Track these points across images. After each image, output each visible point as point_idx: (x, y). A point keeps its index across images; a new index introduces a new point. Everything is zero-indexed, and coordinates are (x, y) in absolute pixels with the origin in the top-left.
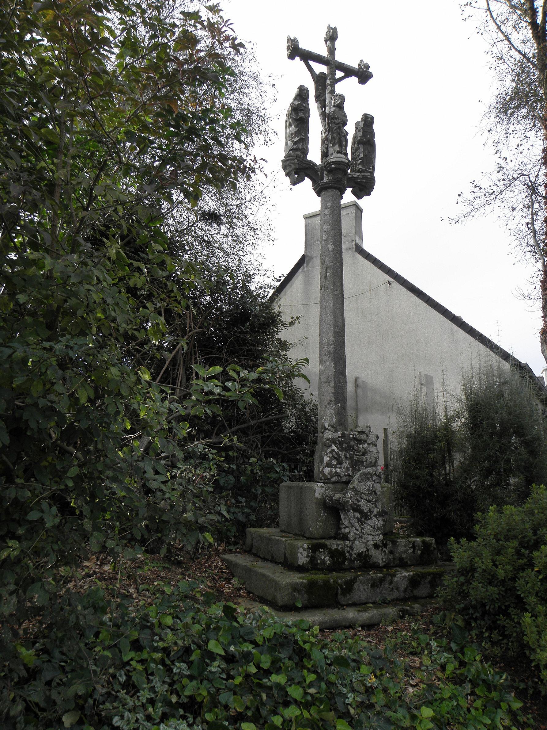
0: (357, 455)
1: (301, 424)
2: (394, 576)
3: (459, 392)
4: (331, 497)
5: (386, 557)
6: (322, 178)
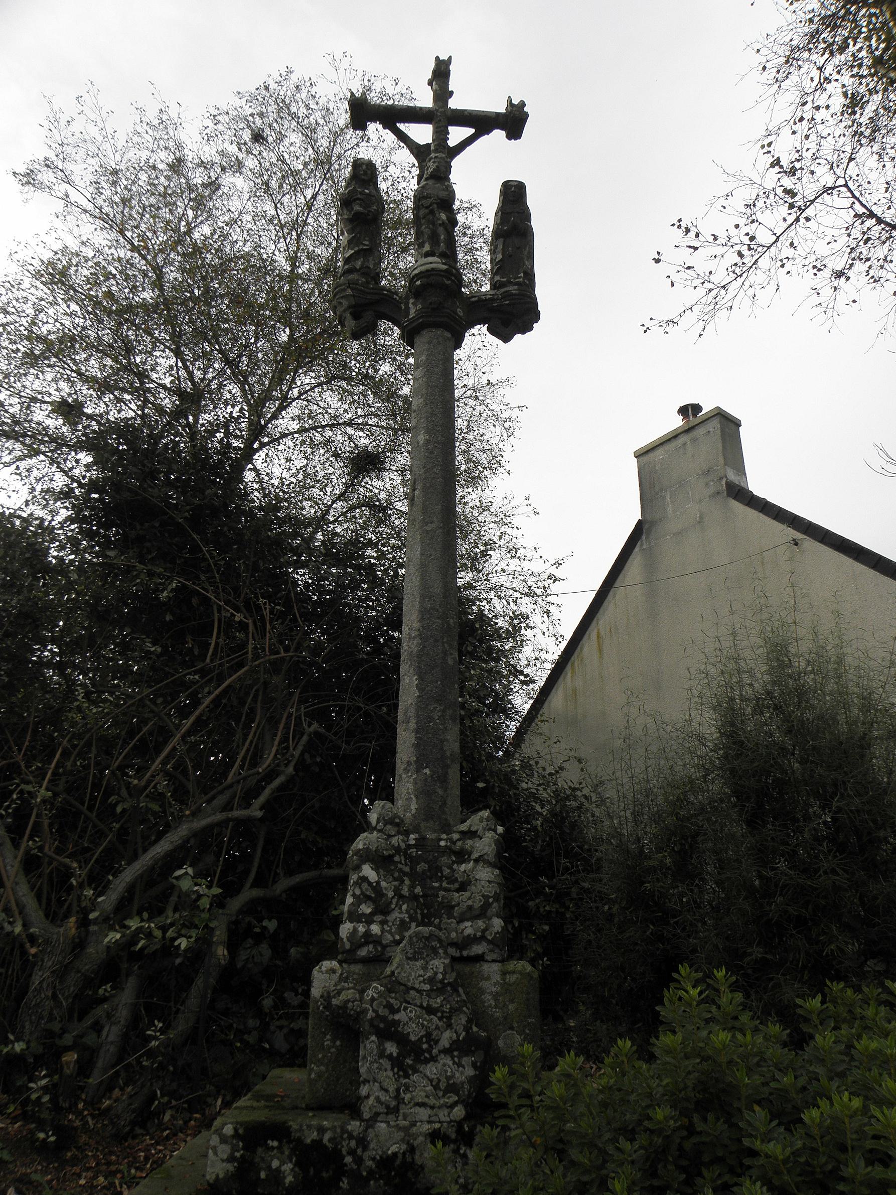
0: (446, 890)
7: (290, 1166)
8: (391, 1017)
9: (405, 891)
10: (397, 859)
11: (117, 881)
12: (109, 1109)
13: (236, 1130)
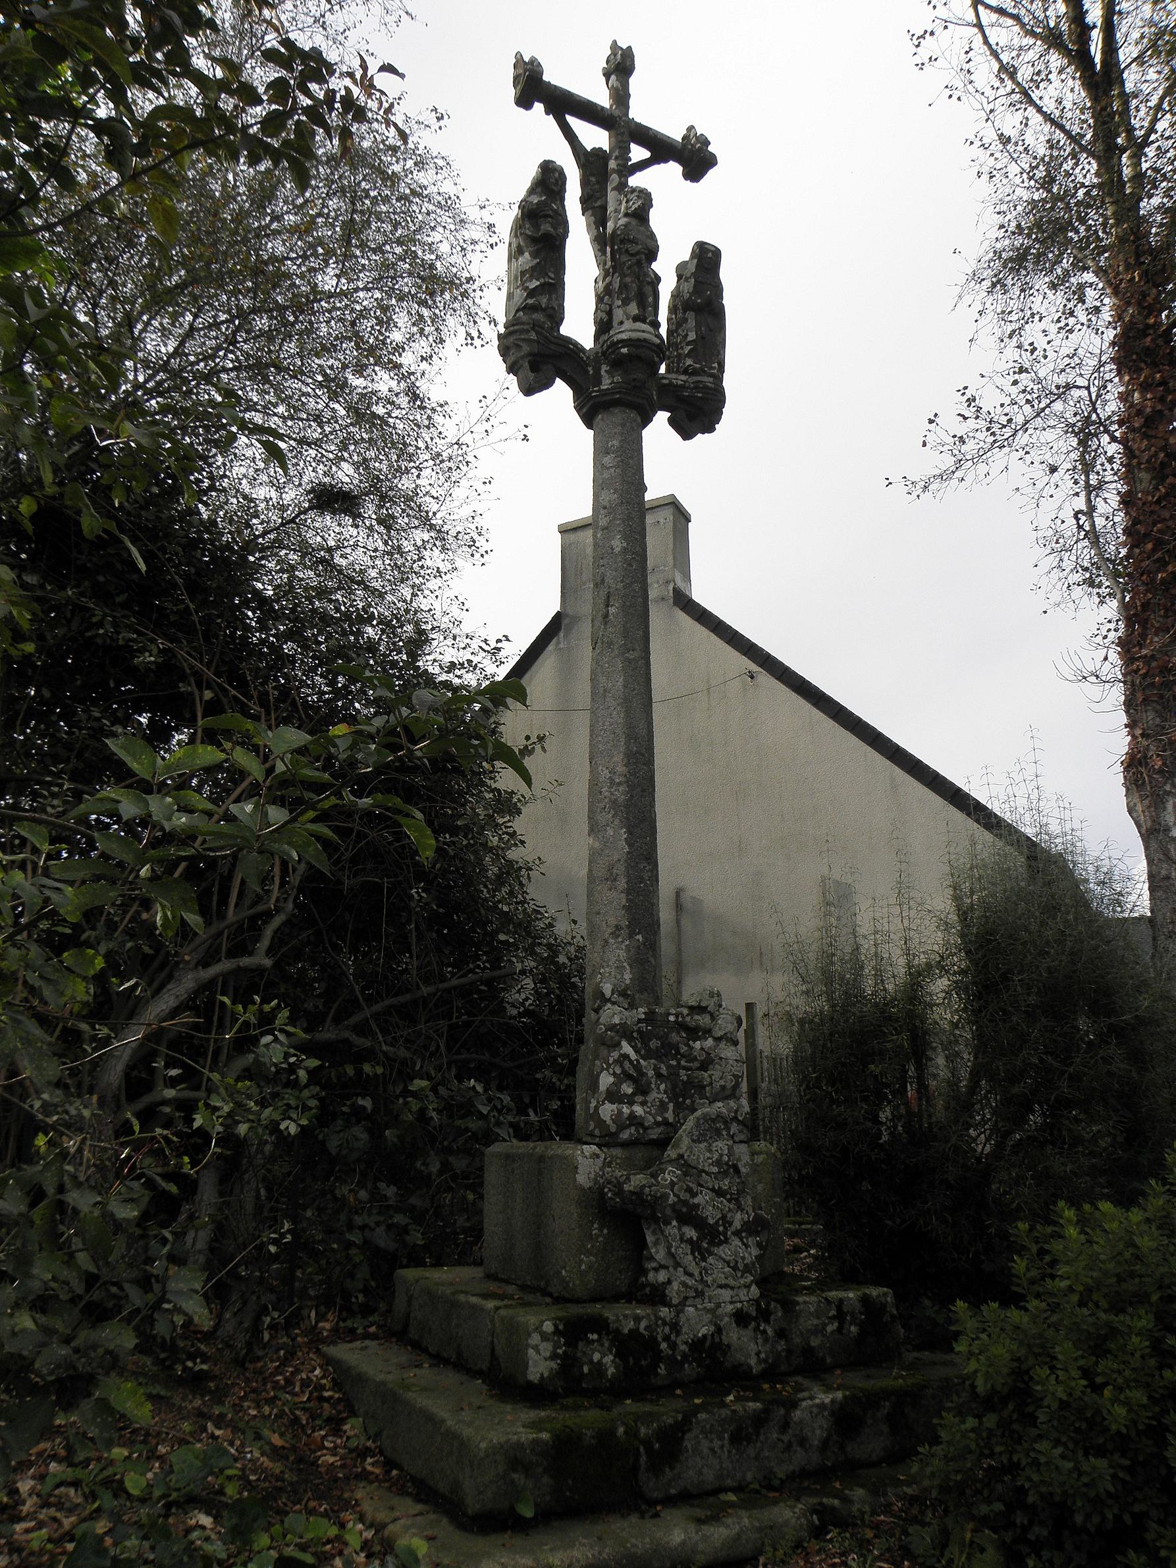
0: (685, 1068)
1: (548, 994)
2: (793, 1404)
3: (942, 903)
4: (619, 1185)
6: (598, 382)
13: (556, 1326)
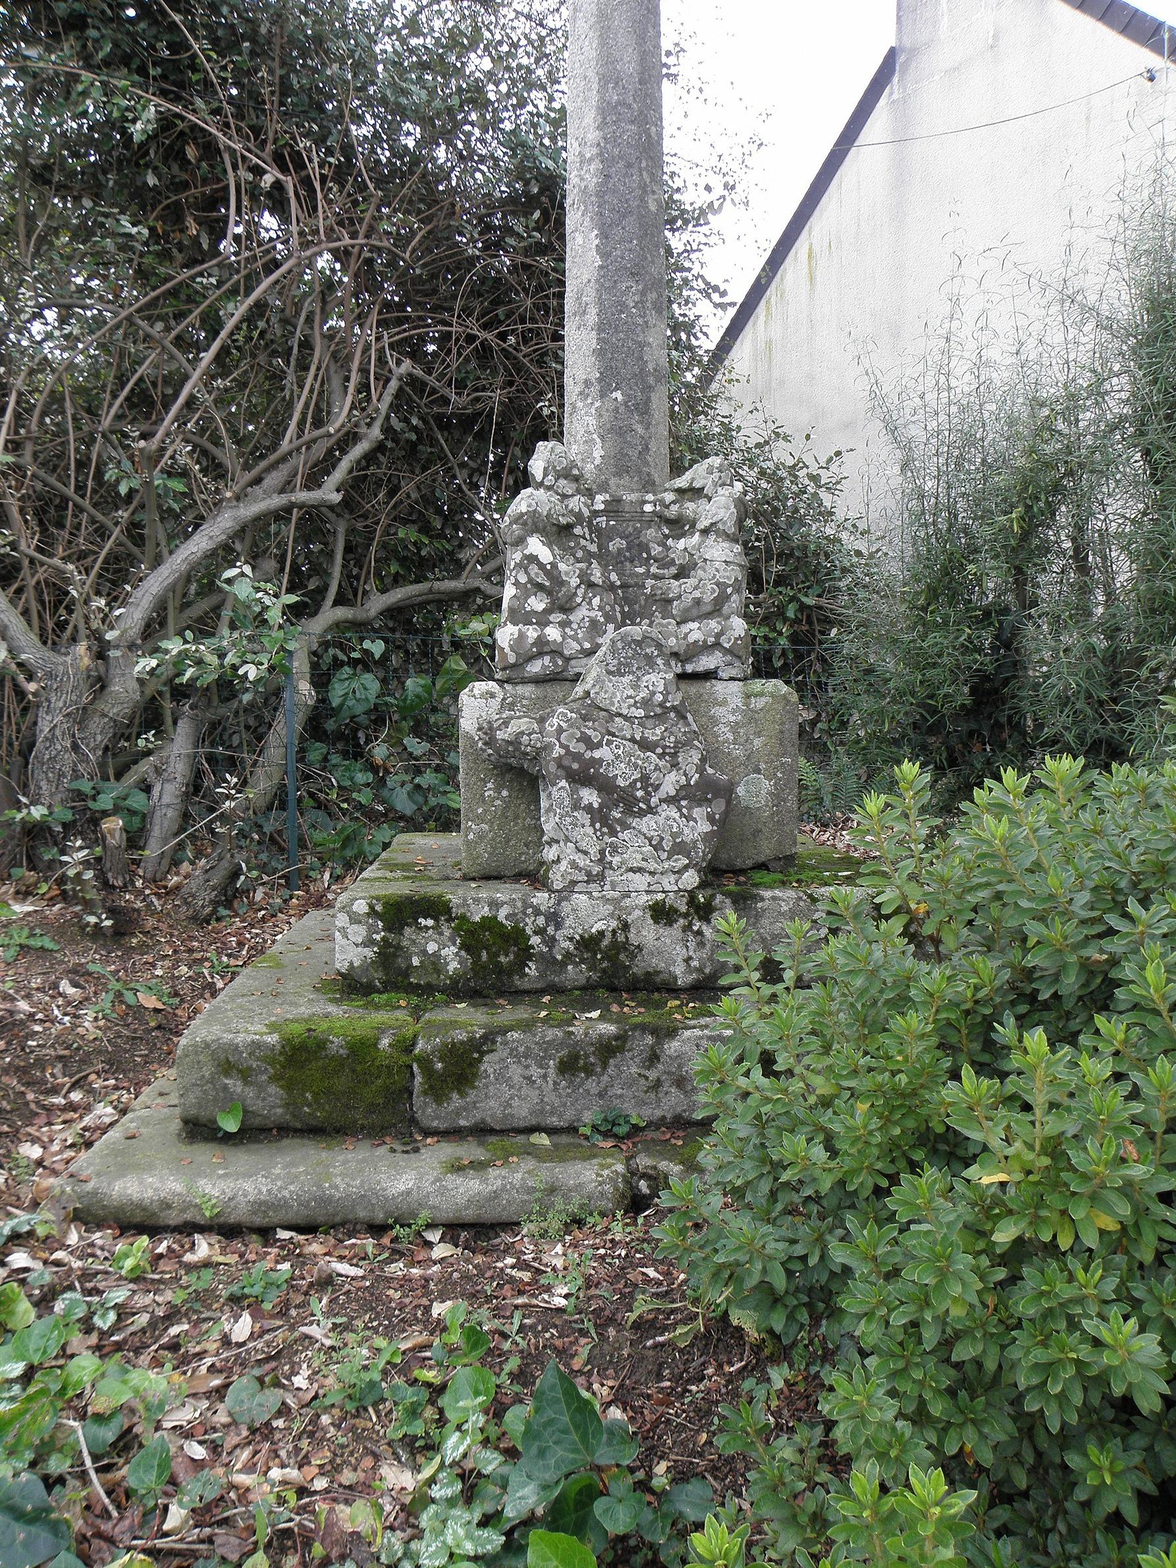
0: (656, 577)
5: (705, 953)
7: (454, 949)
8: (588, 754)
9: (597, 576)
10: (578, 531)
11: (138, 593)
12: (178, 887)
13: (371, 907)
